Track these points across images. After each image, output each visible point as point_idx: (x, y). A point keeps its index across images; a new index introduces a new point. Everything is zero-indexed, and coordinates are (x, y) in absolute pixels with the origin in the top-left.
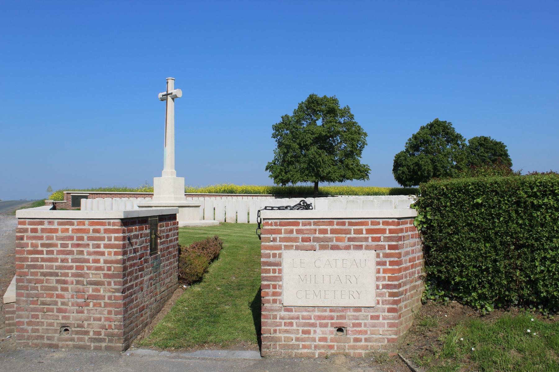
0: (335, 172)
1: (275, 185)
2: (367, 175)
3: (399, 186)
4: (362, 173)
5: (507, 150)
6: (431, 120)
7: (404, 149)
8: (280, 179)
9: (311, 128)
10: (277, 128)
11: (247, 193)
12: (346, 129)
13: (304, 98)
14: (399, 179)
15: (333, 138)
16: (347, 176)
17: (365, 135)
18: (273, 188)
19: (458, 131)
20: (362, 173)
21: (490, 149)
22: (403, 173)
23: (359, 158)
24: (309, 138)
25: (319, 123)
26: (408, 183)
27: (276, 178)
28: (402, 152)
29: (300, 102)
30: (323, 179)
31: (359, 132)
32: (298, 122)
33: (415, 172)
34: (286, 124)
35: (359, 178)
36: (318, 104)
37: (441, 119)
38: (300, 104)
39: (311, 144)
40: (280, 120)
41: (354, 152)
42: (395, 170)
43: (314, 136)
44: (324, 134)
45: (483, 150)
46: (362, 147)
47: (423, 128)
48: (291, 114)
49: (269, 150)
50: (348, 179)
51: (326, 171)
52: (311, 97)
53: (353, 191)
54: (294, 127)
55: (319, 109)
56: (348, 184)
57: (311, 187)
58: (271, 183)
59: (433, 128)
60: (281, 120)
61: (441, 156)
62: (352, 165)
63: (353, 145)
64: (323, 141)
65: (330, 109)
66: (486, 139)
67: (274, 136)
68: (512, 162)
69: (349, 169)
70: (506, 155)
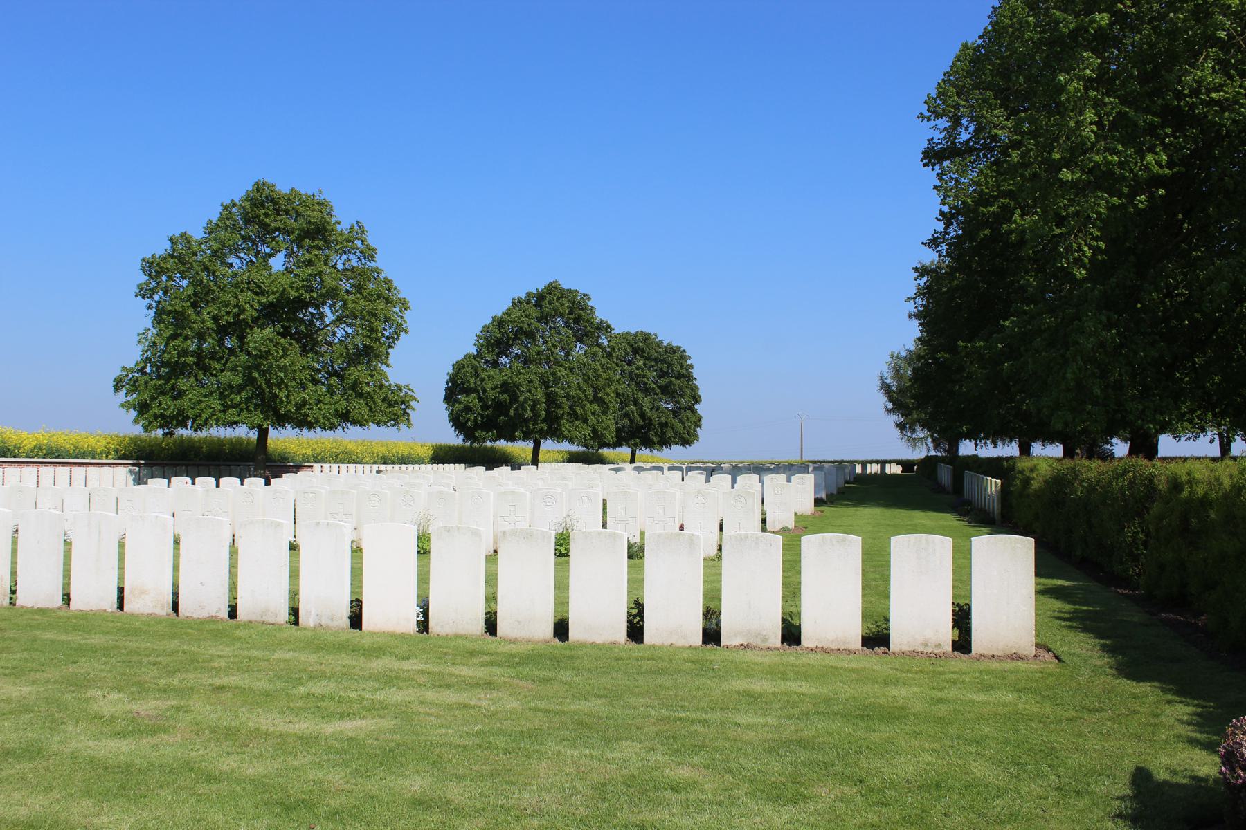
0: (318, 402)
1: (137, 430)
2: (406, 414)
3: (455, 439)
4: (393, 408)
5: (691, 366)
6: (539, 285)
7: (474, 350)
8: (156, 417)
9: (256, 277)
10: (154, 268)
11: (52, 455)
12: (353, 286)
13: (238, 191)
14: (457, 422)
15: (317, 307)
16: (354, 415)
17: (404, 305)
18: (134, 440)
19: (601, 314)
20: (393, 408)
21: (656, 360)
22: (468, 409)
23: (383, 367)
24: (250, 304)
25: (277, 263)
26: (479, 433)
27: (142, 408)
28: (468, 357)
29: (227, 202)
30: (281, 420)
31: (387, 295)
32: (218, 255)
33: (500, 407)
34: (181, 259)
35: (385, 423)
36: (278, 212)
37: (565, 285)
38: (226, 208)
39: (255, 320)
40: (163, 248)
41: (369, 353)
42: (450, 397)
43: (263, 299)
44: (293, 294)
45: (641, 363)
46: (392, 339)
47: (516, 303)
48: (197, 233)
49: (124, 330)
50: (354, 423)
51: (297, 397)
52: (259, 188)
53: (350, 453)
54: (206, 268)
55: (278, 224)
56: (349, 437)
57: (249, 442)
58: (128, 426)
59: (545, 303)
60: (168, 245)
61: (564, 372)
62: (368, 384)
63: (372, 330)
64: (287, 311)
65: (316, 232)
66: (647, 337)
67: (144, 292)
68: (700, 393)
69: (360, 395)
70: (690, 378)
